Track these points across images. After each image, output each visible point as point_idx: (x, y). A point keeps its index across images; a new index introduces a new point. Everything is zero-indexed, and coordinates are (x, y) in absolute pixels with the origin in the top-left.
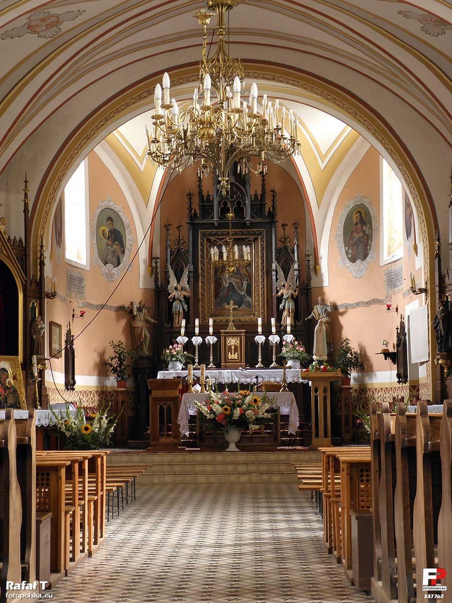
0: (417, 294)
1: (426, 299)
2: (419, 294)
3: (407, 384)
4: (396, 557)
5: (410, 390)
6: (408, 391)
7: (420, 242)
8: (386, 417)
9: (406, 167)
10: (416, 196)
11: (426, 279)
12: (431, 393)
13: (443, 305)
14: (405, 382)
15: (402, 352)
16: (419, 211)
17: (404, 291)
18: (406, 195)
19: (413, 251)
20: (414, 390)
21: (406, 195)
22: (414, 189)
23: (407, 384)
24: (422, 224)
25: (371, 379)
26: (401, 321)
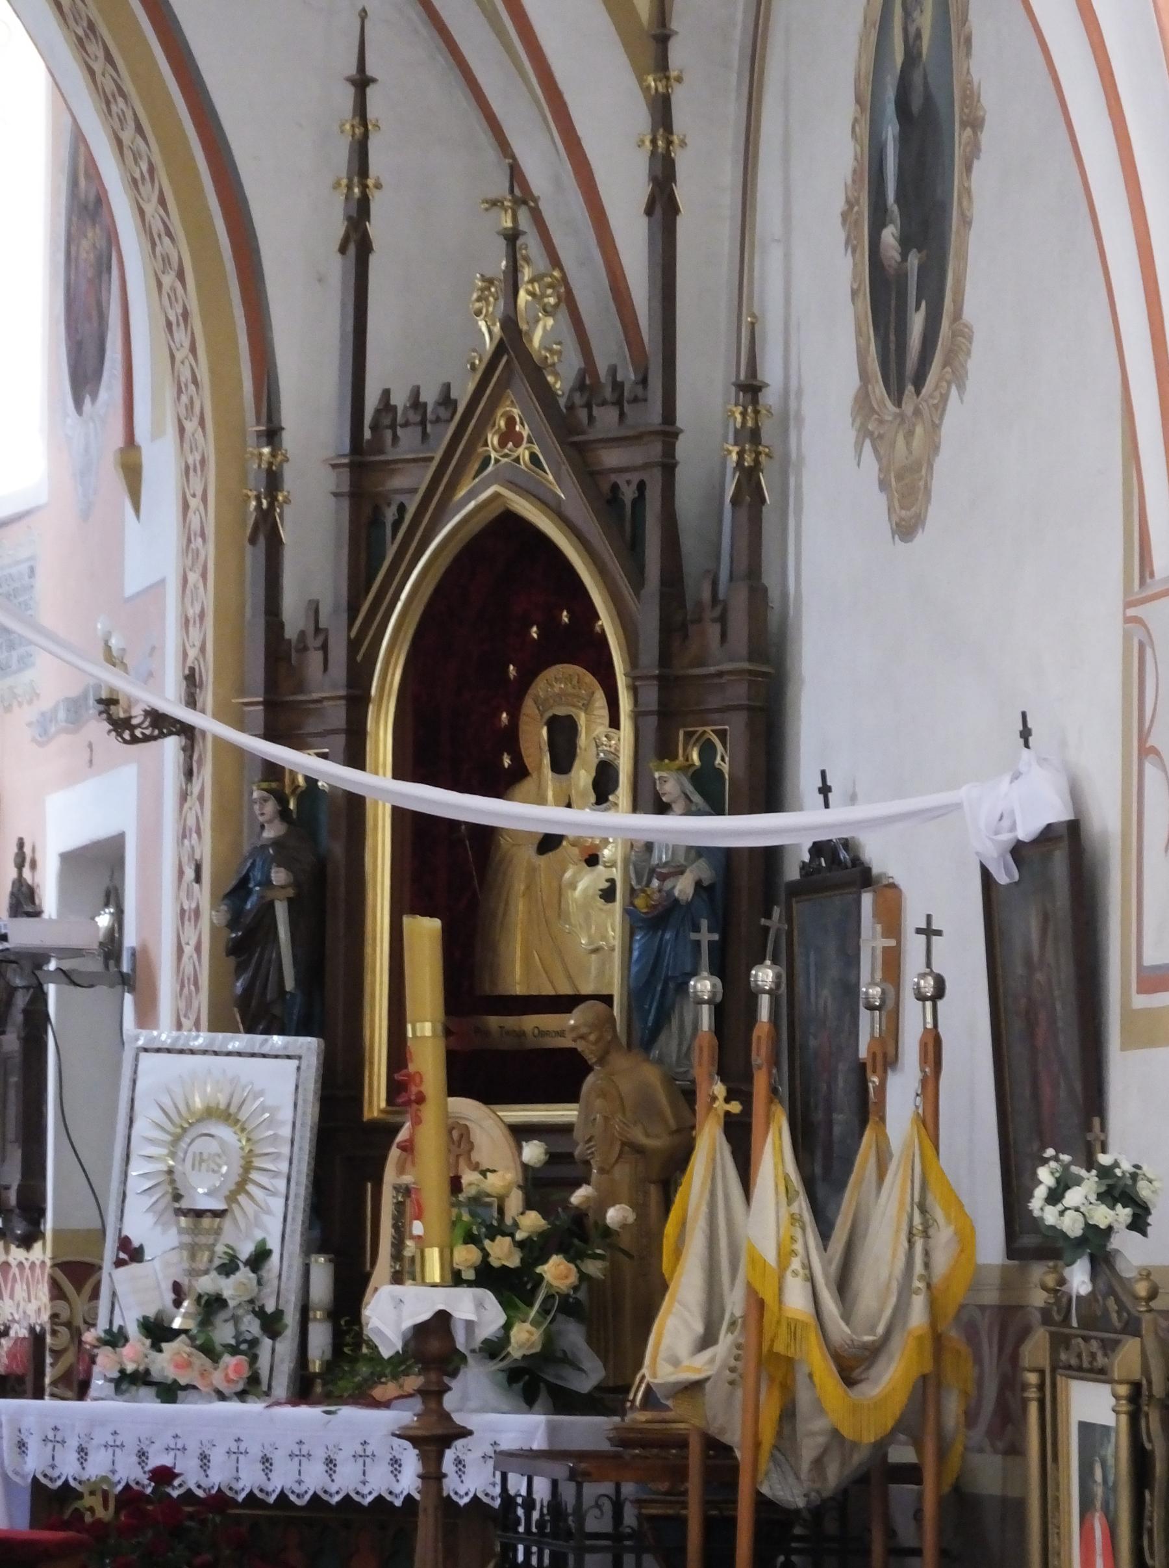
0: (134, 740)
1: (189, 774)
2: (147, 739)
3: (41, 1253)
4: (418, 1218)
5: (57, 1292)
6: (43, 1292)
7: (157, 433)
8: (864, 1015)
9: (217, 440)
10: (152, 169)
11: (192, 653)
12: (1139, 1007)
13: (284, 814)
14: (26, 1242)
15: (17, 1060)
16: (166, 259)
17: (46, 704)
18: (79, 139)
19: (113, 480)
20: (79, 1288)
21: (79, 139)
22: (139, 129)
23: (41, 1253)
24: (181, 336)
25: (625, 1218)
26: (19, 882)
